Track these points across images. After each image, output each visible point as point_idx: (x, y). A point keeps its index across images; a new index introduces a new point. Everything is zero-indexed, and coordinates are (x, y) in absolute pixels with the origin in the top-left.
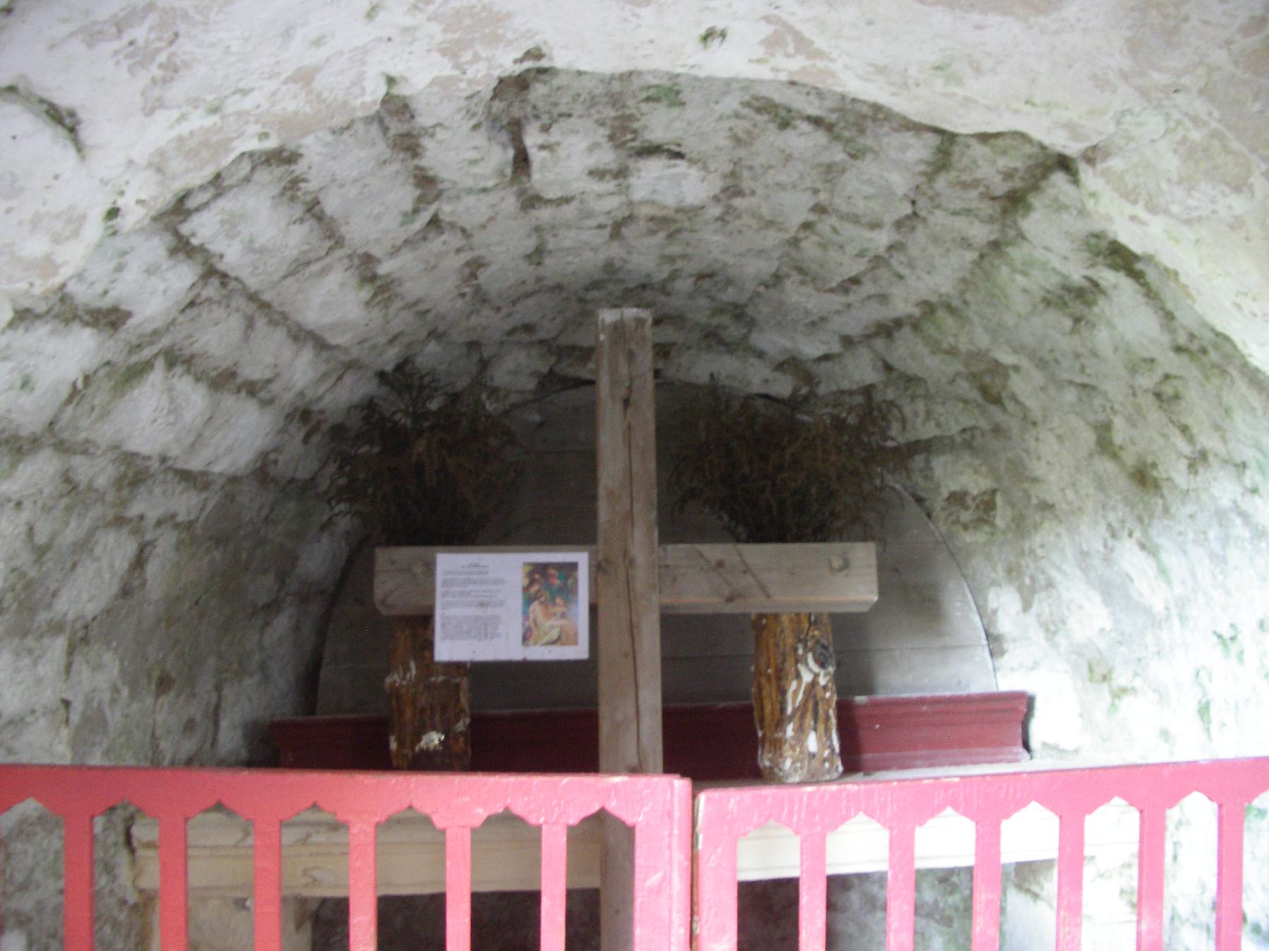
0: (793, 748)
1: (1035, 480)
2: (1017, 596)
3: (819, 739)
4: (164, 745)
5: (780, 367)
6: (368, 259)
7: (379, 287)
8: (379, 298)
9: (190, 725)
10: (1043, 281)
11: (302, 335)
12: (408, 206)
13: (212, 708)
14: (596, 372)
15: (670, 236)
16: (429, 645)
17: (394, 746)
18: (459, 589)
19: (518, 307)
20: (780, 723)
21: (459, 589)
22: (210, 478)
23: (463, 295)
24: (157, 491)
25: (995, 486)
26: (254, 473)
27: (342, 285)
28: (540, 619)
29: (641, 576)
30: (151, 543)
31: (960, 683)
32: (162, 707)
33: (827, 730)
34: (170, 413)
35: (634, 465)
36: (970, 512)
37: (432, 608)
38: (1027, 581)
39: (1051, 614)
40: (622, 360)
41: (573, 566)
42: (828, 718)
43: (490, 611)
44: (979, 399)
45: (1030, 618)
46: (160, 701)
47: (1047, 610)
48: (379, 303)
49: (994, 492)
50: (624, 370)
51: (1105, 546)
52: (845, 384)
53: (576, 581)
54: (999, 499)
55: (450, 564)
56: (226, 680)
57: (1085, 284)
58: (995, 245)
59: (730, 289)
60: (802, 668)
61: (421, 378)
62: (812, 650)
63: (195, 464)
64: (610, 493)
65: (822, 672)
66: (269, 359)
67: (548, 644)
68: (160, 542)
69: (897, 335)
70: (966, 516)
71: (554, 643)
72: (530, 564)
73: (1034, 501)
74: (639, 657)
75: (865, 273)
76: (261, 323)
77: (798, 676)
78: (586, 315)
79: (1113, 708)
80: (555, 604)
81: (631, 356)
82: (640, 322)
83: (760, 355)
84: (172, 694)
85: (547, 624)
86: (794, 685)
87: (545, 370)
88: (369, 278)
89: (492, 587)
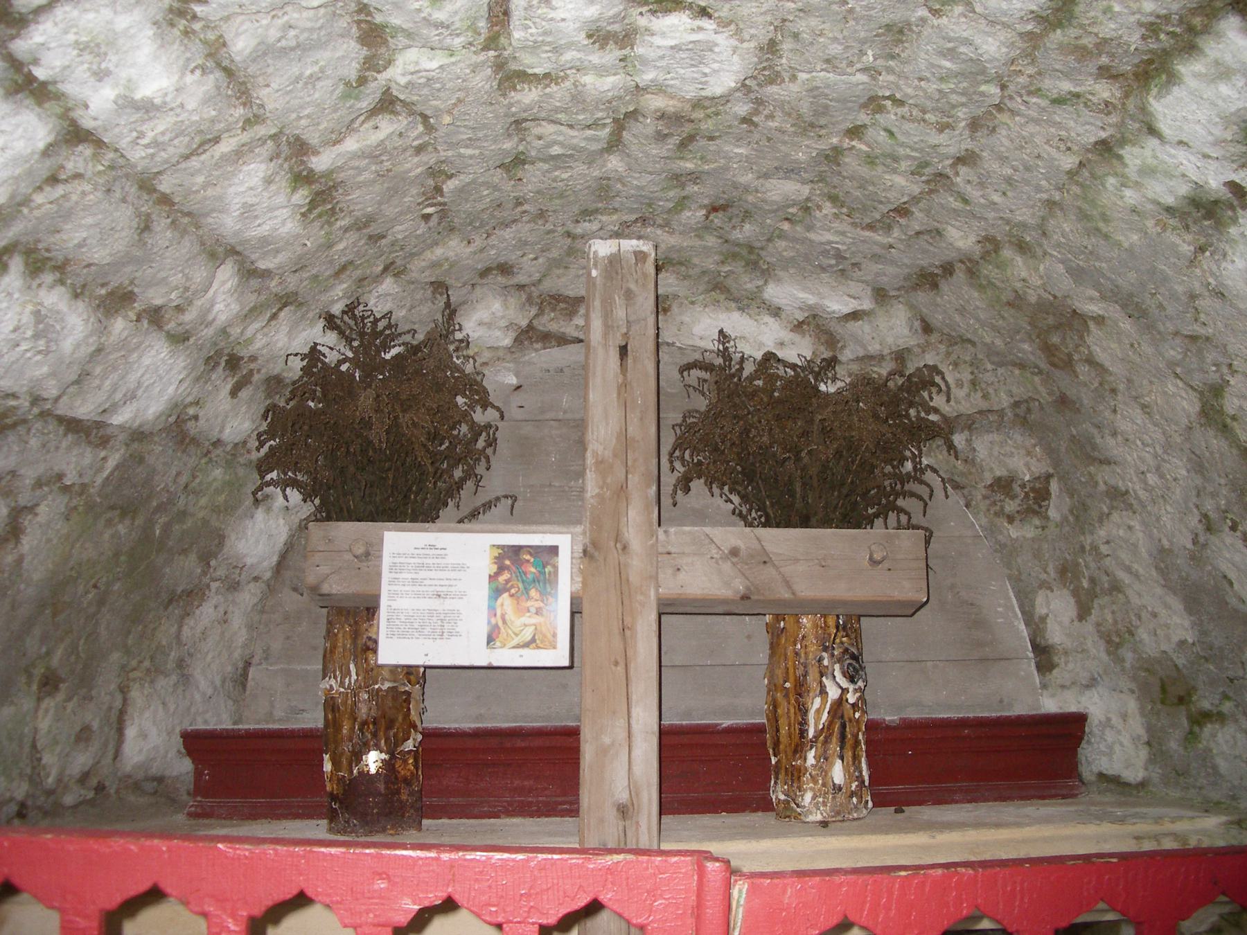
0: (814, 779)
1: (1107, 462)
2: (1072, 601)
3: (846, 769)
4: (47, 759)
5: (799, 327)
6: (301, 148)
7: (318, 194)
8: (316, 212)
9: (84, 735)
10: (1169, 192)
11: (221, 251)
12: (351, 70)
13: (114, 718)
14: (586, 328)
15: (683, 145)
16: (371, 647)
17: (328, 767)
18: (409, 576)
19: (493, 240)
20: (799, 749)
21: (409, 576)
22: (109, 431)
23: (426, 217)
24: (34, 442)
25: (1051, 471)
26: (166, 429)
27: (268, 181)
28: (510, 616)
29: (637, 564)
30: (31, 509)
31: (1001, 701)
32: (47, 711)
33: (856, 758)
34: (36, 336)
35: (630, 429)
36: (1018, 501)
37: (377, 598)
38: (1085, 584)
39: (1116, 622)
40: (618, 300)
41: (554, 550)
42: (857, 743)
43: (448, 604)
44: (1043, 365)
45: (1088, 627)
46: (44, 705)
47: (1109, 618)
48: (320, 216)
49: (1048, 477)
50: (620, 313)
51: (1195, 542)
52: (874, 348)
53: (556, 568)
54: (1054, 486)
55: (400, 544)
56: (134, 680)
57: (1225, 194)
58: (1105, 148)
59: (747, 226)
60: (827, 682)
61: (376, 321)
62: (839, 661)
63: (84, 409)
64: (599, 463)
65: (851, 687)
66: (177, 279)
67: (518, 647)
68: (42, 509)
69: (944, 286)
70: (1011, 506)
71: (526, 645)
72: (498, 547)
73: (1102, 487)
74: (632, 666)
75: (915, 200)
76: (161, 224)
77: (823, 692)
78: (575, 247)
79: (1191, 737)
80: (529, 598)
81: (629, 295)
82: (640, 256)
83: (776, 312)
84: (60, 696)
85: (517, 621)
86: (818, 701)
87: (524, 323)
88: (302, 178)
89: (452, 575)
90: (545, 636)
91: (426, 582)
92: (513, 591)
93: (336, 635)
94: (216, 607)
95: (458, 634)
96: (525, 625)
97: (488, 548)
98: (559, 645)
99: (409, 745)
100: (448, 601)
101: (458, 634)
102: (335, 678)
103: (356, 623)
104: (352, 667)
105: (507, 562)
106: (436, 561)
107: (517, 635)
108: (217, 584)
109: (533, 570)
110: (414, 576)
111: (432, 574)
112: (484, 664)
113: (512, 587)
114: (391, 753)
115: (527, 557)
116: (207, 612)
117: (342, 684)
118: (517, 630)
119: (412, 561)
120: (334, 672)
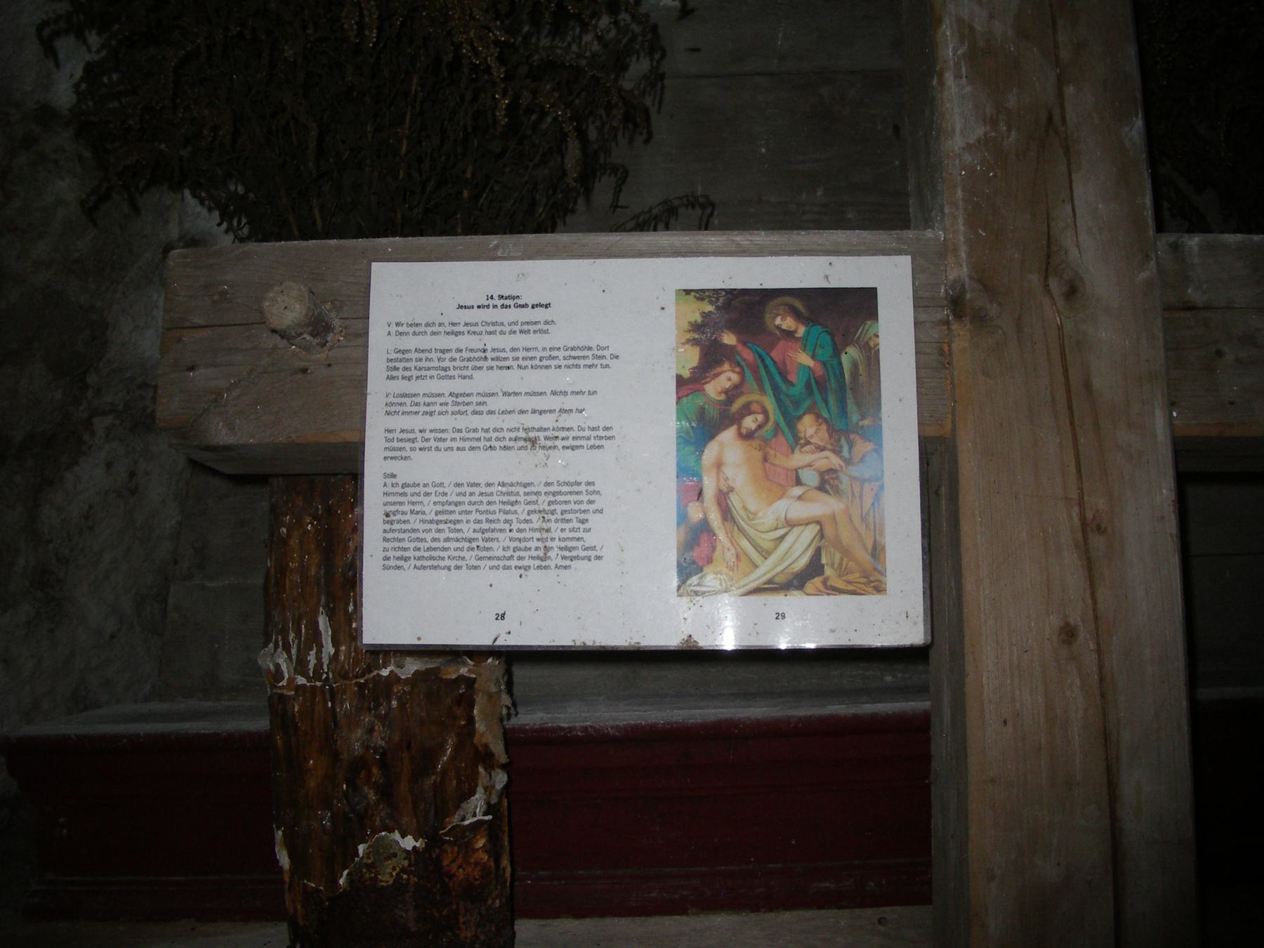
17: (284, 860)
28: (745, 496)
43: (561, 466)
53: (872, 357)
55: (416, 296)
71: (797, 582)
80: (797, 441)
89: (568, 379)
90: (846, 552)
91: (493, 404)
92: (749, 423)
93: (284, 541)
94: (109, 465)
95: (592, 555)
96: (790, 524)
97: (670, 299)
98: (891, 581)
99: (475, 809)
100: (559, 459)
101: (592, 555)
102: (287, 648)
103: (329, 511)
104: (323, 621)
105: (729, 339)
106: (520, 341)
107: (765, 554)
108: (108, 420)
109: (804, 359)
110: (458, 386)
111: (511, 380)
112: (671, 640)
113: (747, 410)
114: (433, 839)
115: (788, 323)
116: (90, 477)
117: (301, 666)
118: (765, 540)
119: (452, 342)
120: (284, 632)
